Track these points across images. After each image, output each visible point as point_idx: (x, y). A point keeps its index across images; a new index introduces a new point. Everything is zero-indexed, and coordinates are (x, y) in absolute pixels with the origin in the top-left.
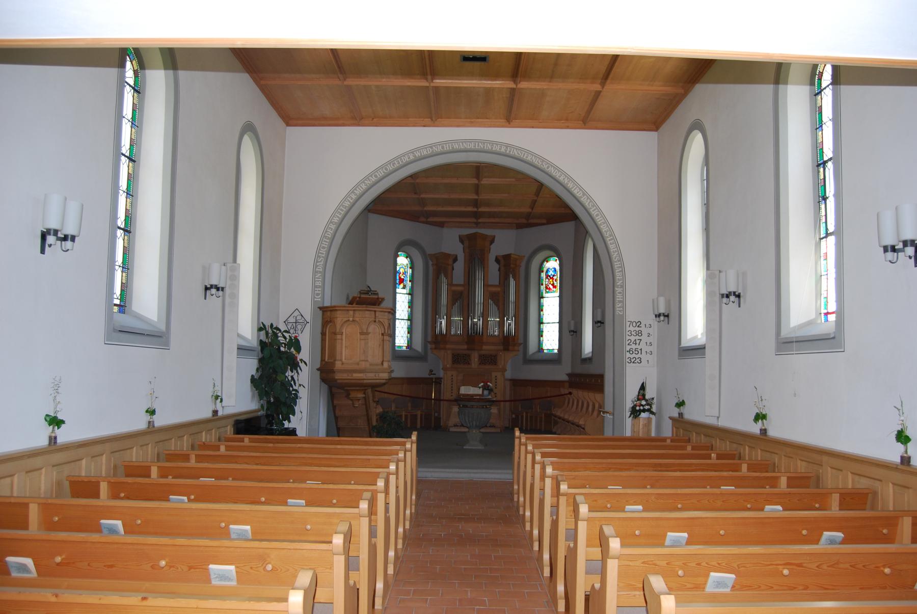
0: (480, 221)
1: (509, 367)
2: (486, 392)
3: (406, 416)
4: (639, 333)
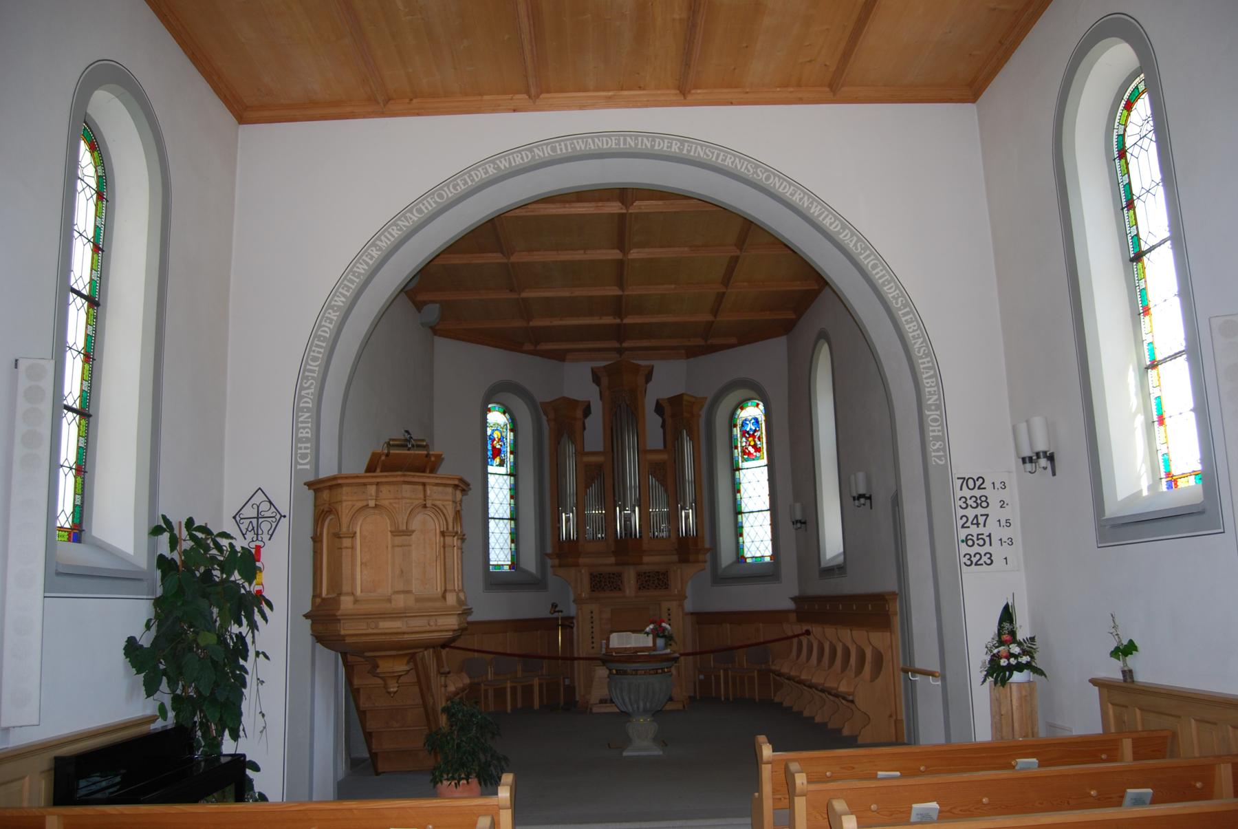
0: (625, 345)
1: (689, 591)
2: (660, 642)
3: (514, 689)
4: (982, 502)
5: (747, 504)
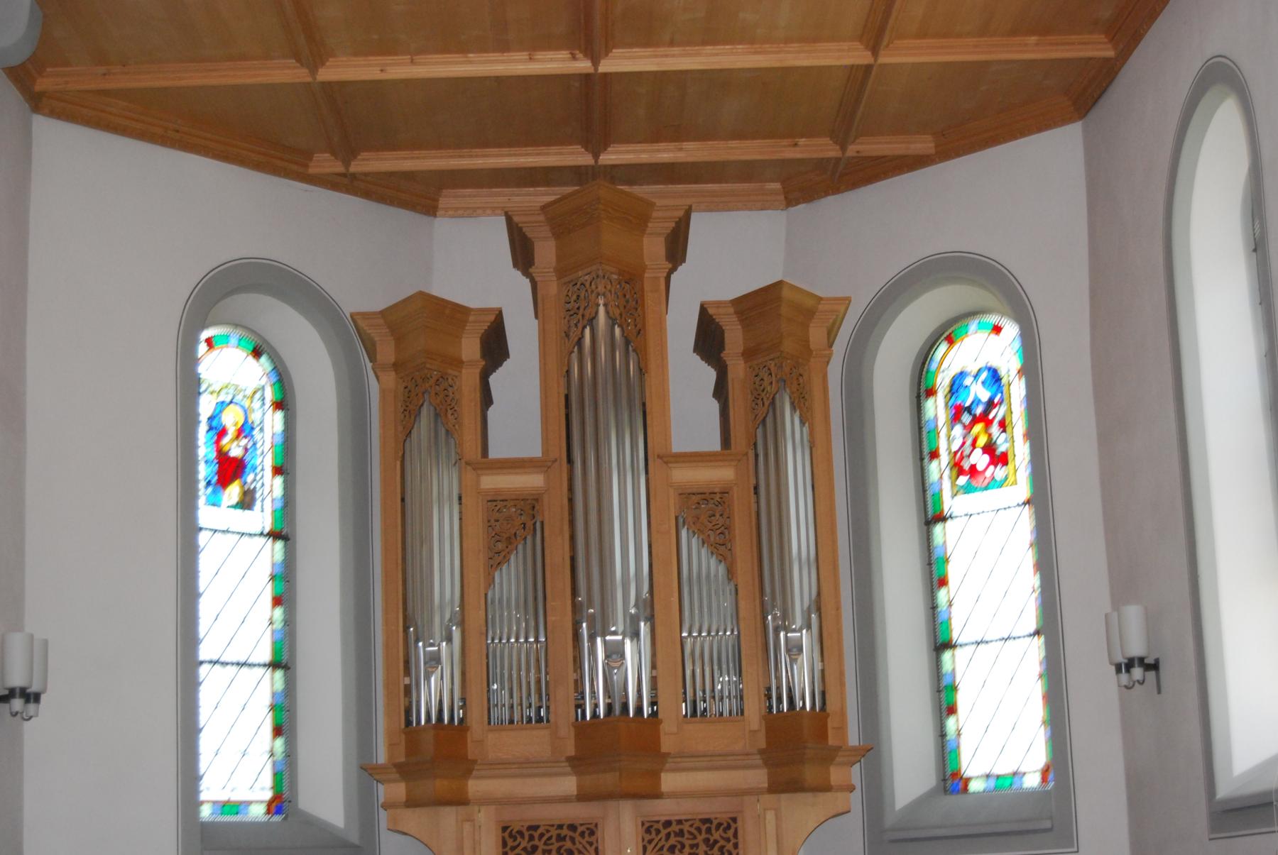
0: (612, 156)
5: (262, 688)
